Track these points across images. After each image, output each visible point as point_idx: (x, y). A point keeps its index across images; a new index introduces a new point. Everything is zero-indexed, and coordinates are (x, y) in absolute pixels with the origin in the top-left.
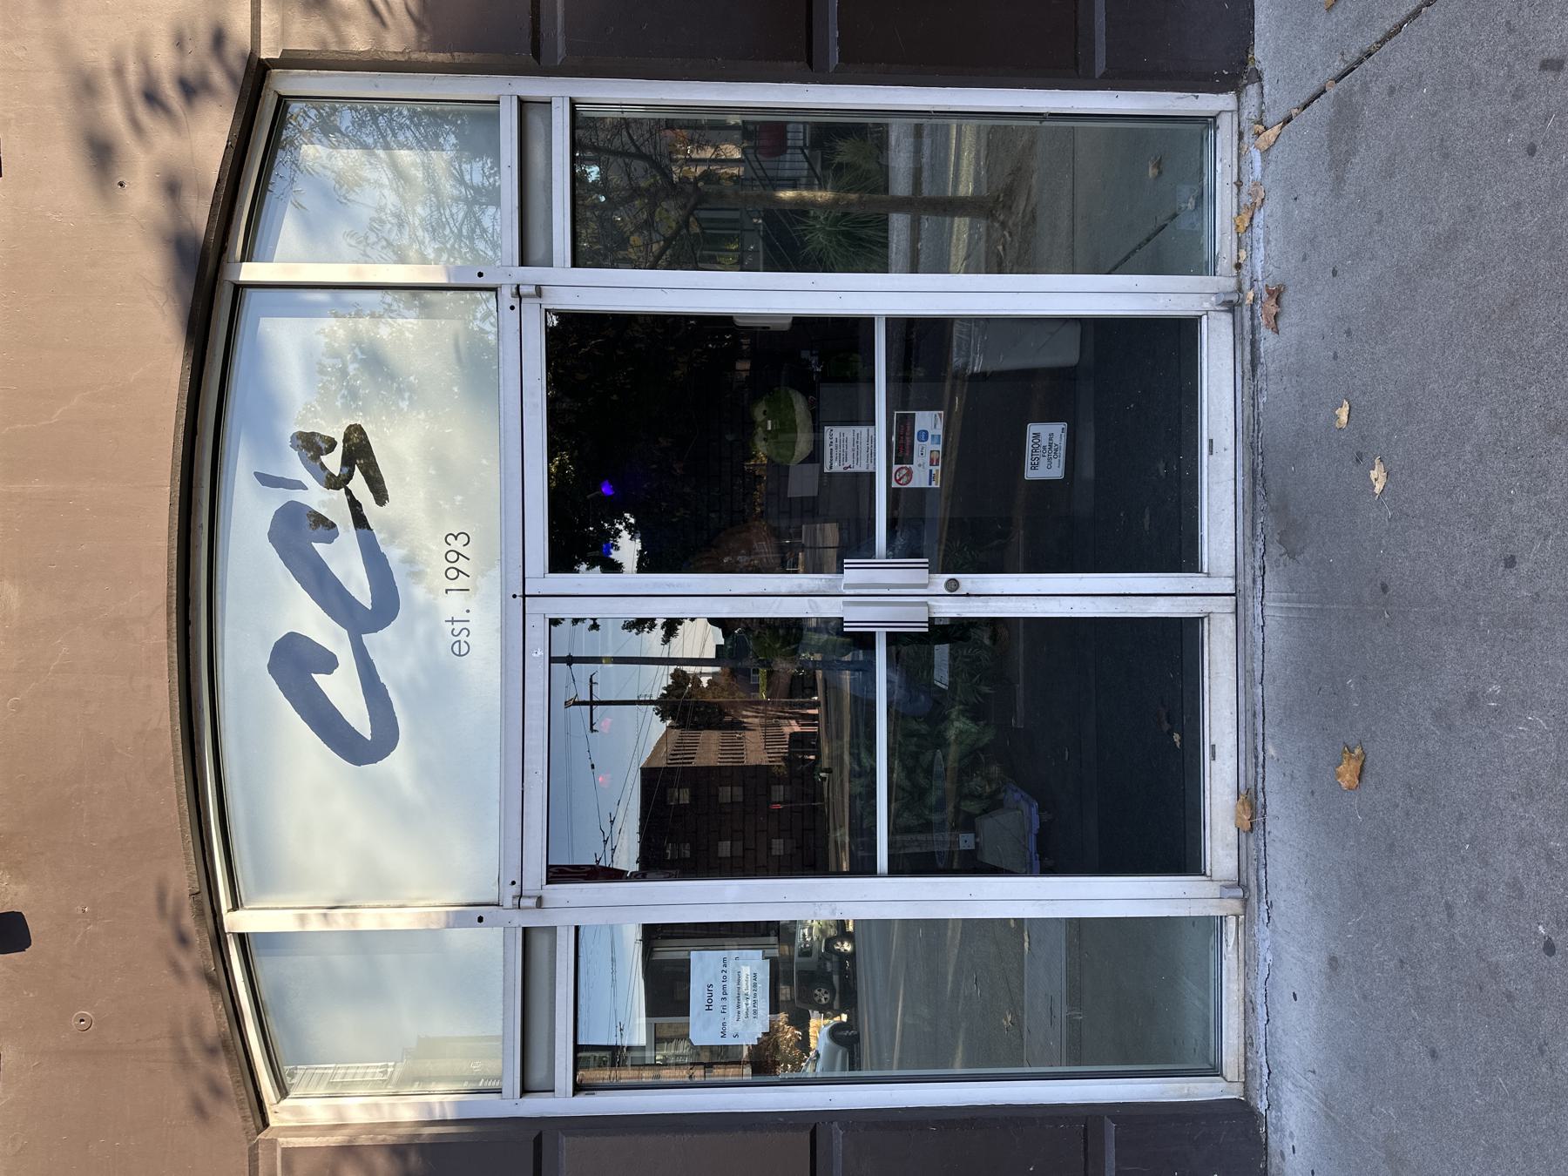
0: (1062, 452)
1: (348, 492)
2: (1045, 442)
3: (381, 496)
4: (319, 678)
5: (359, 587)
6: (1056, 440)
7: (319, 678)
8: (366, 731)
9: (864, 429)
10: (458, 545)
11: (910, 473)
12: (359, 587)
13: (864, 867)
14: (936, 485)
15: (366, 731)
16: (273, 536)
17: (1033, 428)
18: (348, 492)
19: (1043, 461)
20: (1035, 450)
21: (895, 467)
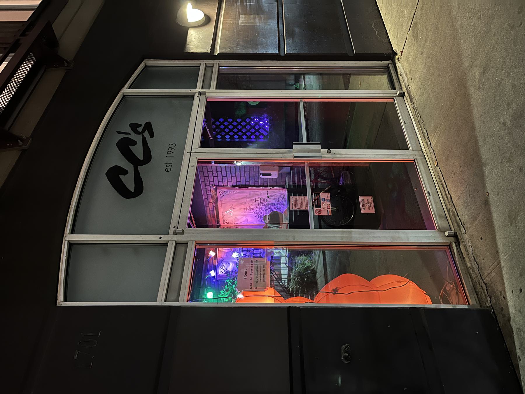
0: (373, 204)
1: (143, 136)
2: (366, 202)
3: (152, 135)
4: (122, 177)
5: (140, 155)
6: (370, 201)
7: (122, 177)
8: (141, 158)
9: (302, 197)
10: (172, 146)
11: (320, 211)
12: (140, 155)
13: (308, 106)
14: (330, 214)
15: (141, 158)
16: (106, 174)
17: (363, 211)
18: (143, 136)
19: (367, 207)
20: (363, 204)
21: (315, 209)
